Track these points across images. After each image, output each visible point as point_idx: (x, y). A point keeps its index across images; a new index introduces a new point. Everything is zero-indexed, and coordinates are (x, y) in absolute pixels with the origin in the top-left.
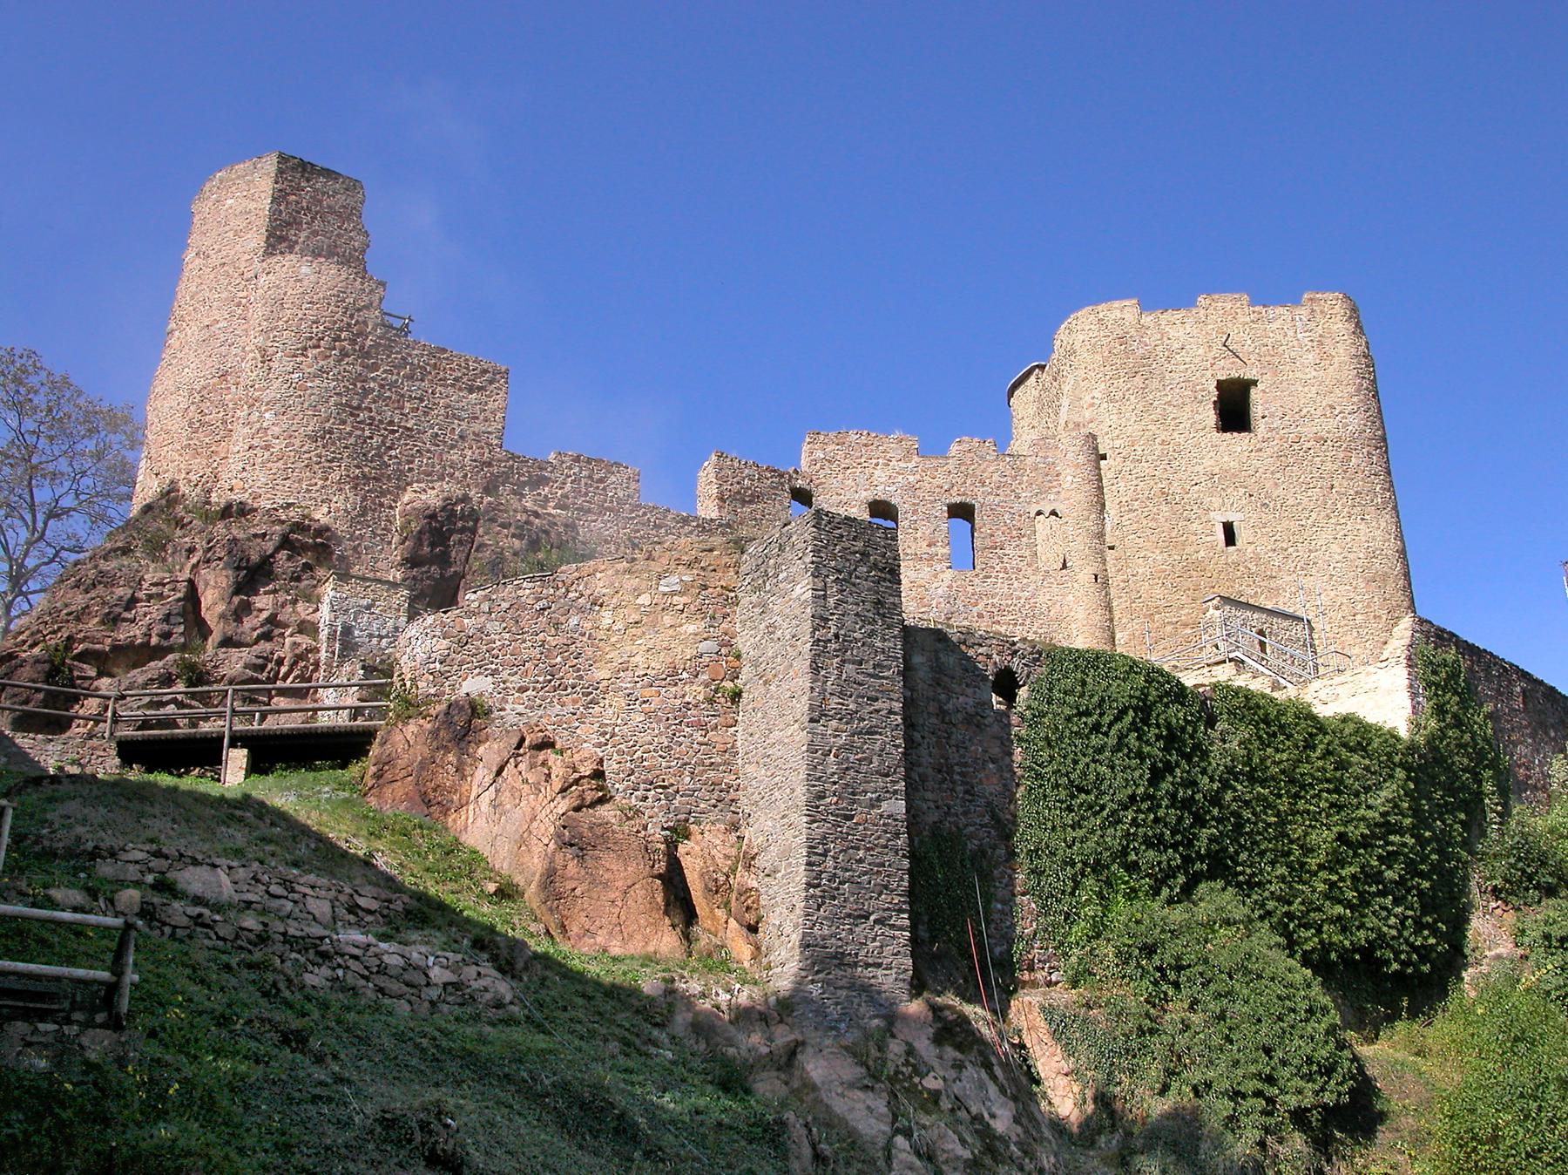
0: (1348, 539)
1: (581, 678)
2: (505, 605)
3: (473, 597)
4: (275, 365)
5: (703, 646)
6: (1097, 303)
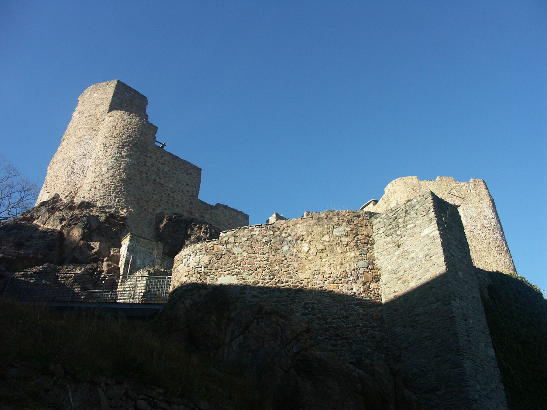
0: (498, 261)
1: (292, 278)
2: (244, 239)
3: (224, 235)
4: (109, 150)
5: (360, 264)
6: (404, 176)
